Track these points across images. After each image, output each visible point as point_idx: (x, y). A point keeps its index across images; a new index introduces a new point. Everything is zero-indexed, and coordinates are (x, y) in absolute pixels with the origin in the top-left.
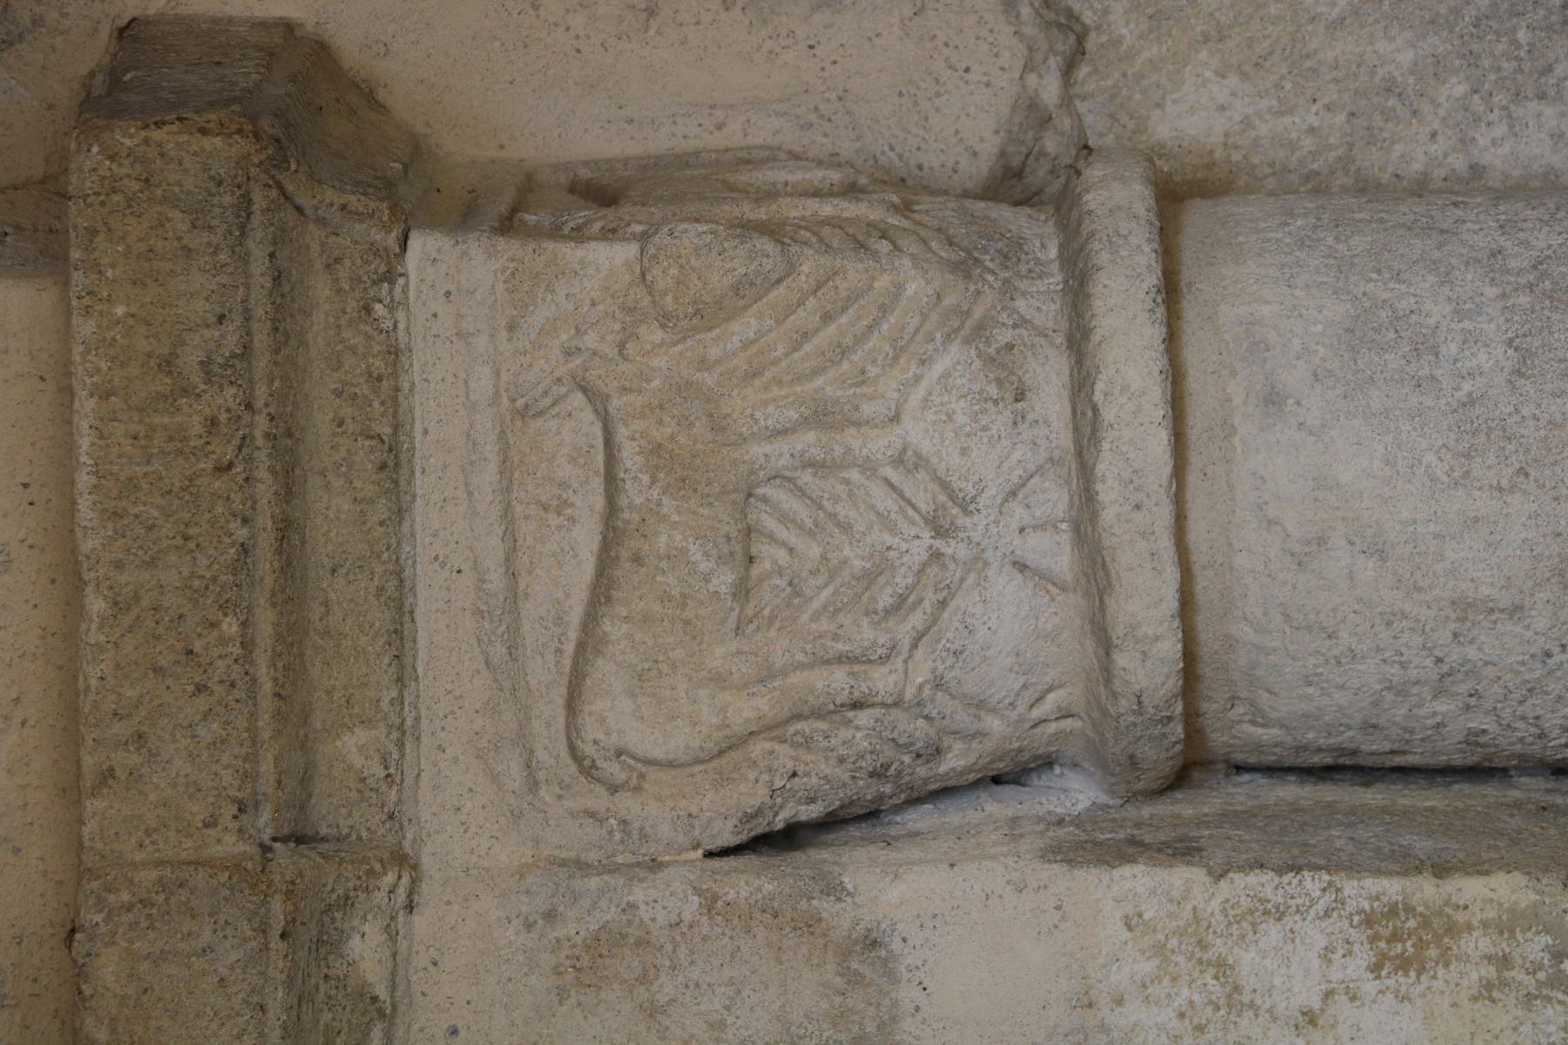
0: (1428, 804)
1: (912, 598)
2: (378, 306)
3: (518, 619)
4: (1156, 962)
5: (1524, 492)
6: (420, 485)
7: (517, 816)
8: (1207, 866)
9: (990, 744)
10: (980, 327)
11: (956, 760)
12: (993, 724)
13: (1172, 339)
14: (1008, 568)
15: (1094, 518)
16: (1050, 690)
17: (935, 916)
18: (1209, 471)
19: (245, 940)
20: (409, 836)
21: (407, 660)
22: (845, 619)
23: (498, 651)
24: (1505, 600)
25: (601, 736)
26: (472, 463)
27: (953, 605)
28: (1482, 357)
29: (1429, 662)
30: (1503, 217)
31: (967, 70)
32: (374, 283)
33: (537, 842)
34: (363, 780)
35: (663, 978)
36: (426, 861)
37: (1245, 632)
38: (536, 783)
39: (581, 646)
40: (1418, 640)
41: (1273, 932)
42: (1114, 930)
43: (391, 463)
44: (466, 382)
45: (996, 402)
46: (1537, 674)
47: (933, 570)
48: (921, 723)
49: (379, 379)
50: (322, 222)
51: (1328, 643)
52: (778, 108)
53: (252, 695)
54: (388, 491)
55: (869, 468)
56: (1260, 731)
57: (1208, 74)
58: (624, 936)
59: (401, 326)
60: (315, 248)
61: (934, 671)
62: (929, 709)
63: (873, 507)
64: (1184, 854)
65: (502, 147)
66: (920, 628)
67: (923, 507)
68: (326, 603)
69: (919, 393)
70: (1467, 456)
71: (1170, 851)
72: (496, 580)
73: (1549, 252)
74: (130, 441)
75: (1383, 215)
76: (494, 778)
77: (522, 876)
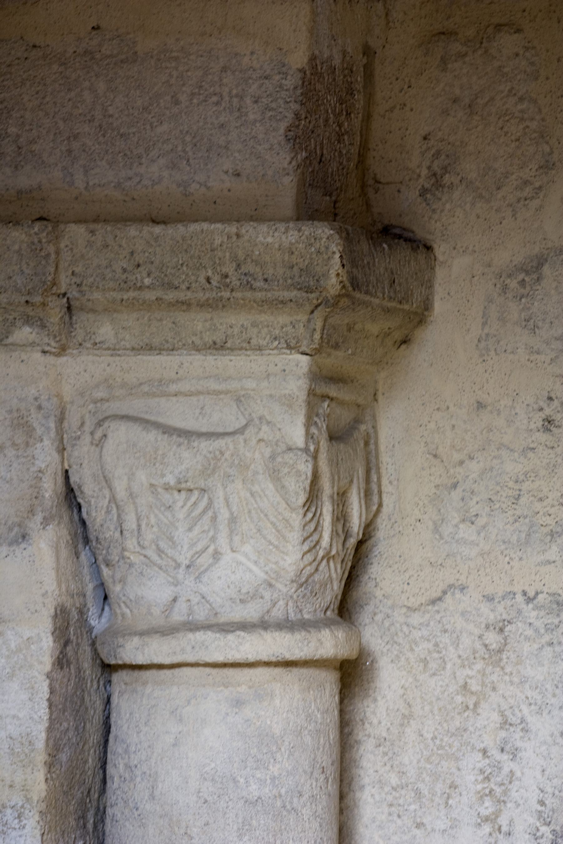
0: (90, 760)
1: (163, 556)
2: (277, 342)
3: (158, 396)
4: (15, 650)
5: (197, 802)
6: (210, 358)
7: (82, 394)
8: (52, 671)
9: (111, 586)
10: (271, 585)
11: (106, 571)
12: (118, 588)
13: (268, 664)
14: (174, 595)
15: (191, 630)
16: (131, 611)
17: (34, 561)
18: (211, 677)
19: (25, 287)
20: (74, 352)
21: (142, 352)
22: (155, 529)
23: (146, 388)
24: (157, 793)
25: (111, 428)
26: (219, 379)
27: (161, 572)
28: (254, 787)
29: (136, 762)
30: (318, 797)
31: (408, 584)
32: (286, 341)
33: (72, 403)
34: (94, 334)
35: (14, 452)
36: (64, 359)
37: (149, 689)
38: (95, 403)
39: (147, 422)
40: (143, 758)
41: (24, 696)
42: (27, 634)
43: (217, 346)
44: (250, 377)
45: (240, 591)
46: (131, 804)
47: (173, 564)
48: (117, 558)
49: (249, 342)
50: (309, 321)
51: (144, 723)
52: (397, 506)
53: (121, 290)
54: (206, 345)
55: (213, 539)
56: (117, 694)
57: (403, 681)
58: (31, 437)
59: (271, 352)
60: (299, 318)
61: (135, 564)
62: (122, 561)
63: (199, 540)
64: (59, 662)
65: (383, 394)
66: (151, 559)
67: (198, 561)
68: (161, 320)
69: (243, 559)
70: (213, 780)
71: (61, 656)
72: (173, 388)
73: (300, 814)
74: (219, 243)
75: (321, 749)
76: (97, 386)
77: (57, 396)
